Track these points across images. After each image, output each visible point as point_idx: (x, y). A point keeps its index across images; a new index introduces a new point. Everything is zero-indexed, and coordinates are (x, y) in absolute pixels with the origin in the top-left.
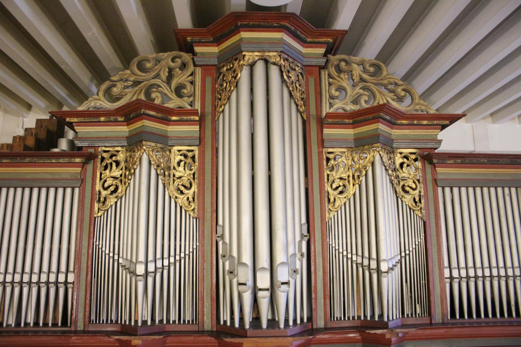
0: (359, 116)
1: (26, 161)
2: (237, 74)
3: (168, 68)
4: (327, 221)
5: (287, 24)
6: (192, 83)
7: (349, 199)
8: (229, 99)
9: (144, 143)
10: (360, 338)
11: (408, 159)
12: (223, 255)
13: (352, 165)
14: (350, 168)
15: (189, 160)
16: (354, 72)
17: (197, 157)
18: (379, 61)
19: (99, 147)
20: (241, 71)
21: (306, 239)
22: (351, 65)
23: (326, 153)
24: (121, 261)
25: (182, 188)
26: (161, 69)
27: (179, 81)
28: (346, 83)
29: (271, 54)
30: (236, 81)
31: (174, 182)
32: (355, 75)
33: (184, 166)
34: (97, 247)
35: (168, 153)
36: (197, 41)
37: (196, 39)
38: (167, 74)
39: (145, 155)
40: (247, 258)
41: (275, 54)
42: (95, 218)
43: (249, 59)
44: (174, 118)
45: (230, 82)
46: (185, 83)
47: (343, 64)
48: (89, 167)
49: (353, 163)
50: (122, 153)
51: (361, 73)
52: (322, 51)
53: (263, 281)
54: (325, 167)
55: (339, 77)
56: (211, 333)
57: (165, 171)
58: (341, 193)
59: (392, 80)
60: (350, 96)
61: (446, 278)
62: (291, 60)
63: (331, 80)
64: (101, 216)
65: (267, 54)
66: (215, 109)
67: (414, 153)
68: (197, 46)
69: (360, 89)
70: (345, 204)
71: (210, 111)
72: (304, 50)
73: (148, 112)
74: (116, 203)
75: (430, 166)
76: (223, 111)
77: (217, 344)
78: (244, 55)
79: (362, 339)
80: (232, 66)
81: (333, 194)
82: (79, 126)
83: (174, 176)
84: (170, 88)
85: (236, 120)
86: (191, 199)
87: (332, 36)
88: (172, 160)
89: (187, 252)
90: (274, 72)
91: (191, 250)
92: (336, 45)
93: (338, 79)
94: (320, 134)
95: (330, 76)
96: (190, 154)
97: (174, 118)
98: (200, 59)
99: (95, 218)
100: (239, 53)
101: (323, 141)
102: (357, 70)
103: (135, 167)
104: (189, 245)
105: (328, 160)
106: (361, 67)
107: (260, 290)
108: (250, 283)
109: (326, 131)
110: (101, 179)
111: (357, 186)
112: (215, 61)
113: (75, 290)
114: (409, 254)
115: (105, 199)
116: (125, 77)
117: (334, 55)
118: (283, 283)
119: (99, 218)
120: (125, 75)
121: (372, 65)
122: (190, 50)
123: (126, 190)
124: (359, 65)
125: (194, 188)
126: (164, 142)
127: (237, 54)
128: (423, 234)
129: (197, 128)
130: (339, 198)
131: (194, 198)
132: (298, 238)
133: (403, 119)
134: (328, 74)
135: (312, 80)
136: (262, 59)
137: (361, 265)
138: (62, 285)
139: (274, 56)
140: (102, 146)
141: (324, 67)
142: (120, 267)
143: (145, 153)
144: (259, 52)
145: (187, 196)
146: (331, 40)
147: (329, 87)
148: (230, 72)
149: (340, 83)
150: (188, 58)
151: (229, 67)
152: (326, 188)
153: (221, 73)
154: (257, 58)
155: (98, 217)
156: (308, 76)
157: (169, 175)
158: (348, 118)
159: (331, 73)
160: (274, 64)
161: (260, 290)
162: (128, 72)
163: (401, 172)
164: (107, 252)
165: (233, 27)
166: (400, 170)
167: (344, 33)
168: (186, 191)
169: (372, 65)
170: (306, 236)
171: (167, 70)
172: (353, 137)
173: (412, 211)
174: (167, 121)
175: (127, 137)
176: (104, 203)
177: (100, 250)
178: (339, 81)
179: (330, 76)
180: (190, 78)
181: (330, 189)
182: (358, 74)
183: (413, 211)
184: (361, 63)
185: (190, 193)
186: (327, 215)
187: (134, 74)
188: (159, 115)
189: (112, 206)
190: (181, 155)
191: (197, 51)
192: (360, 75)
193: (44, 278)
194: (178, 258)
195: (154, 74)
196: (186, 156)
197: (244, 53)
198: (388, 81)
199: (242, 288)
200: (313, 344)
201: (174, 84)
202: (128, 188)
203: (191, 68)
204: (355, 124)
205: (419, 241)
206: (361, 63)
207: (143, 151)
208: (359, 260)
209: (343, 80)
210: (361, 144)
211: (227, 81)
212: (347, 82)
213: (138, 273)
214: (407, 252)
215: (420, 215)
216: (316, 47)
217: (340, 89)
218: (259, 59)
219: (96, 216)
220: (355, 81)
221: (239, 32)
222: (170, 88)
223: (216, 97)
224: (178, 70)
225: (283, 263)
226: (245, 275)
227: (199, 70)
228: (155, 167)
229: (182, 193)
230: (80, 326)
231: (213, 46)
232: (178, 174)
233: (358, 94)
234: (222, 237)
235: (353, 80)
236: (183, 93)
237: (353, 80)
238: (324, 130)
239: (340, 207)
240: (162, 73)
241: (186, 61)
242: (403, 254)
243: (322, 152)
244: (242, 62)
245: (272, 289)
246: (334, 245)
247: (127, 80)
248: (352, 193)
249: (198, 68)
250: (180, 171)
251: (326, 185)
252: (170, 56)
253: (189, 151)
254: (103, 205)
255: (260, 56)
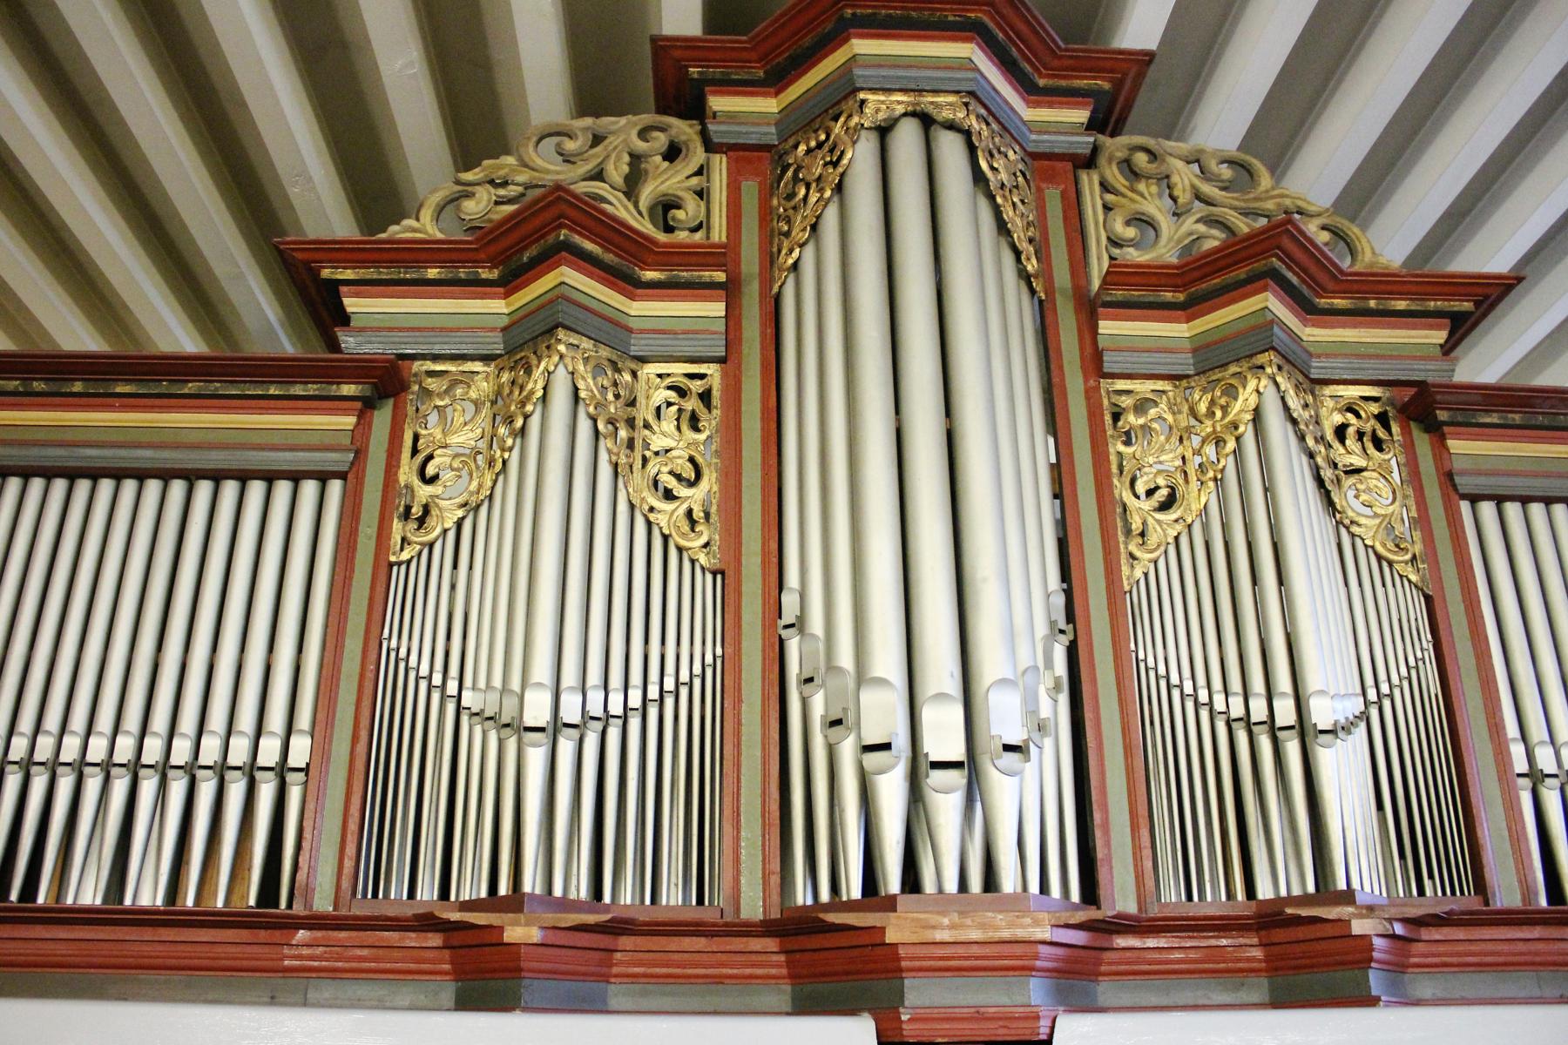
0: (1202, 278)
1: (186, 391)
2: (842, 153)
3: (631, 155)
4: (1127, 588)
5: (986, 20)
6: (700, 194)
7: (1189, 526)
8: (814, 227)
9: (561, 334)
10: (1257, 953)
11: (1358, 416)
12: (806, 675)
13: (1189, 429)
14: (1185, 436)
15: (691, 404)
16: (1175, 179)
17: (716, 393)
18: (1246, 153)
19: (413, 357)
20: (854, 143)
21: (1065, 640)
22: (1164, 161)
23: (1108, 392)
24: (468, 699)
25: (672, 483)
26: (608, 156)
27: (663, 188)
28: (1154, 206)
29: (940, 99)
30: (841, 170)
31: (644, 466)
32: (1180, 186)
33: (678, 420)
34: (393, 655)
35: (627, 377)
36: (718, 76)
37: (715, 72)
38: (626, 169)
39: (564, 369)
40: (887, 660)
41: (951, 99)
42: (391, 565)
43: (878, 111)
44: (650, 275)
45: (819, 180)
46: (680, 193)
47: (1141, 159)
48: (382, 418)
49: (1193, 422)
50: (486, 379)
51: (1197, 182)
52: (1081, 115)
53: (944, 740)
54: (1110, 432)
55: (1133, 190)
56: (767, 928)
57: (627, 419)
58: (1165, 506)
59: (1288, 202)
60: (1170, 240)
61: (1519, 775)
62: (995, 126)
63: (1109, 197)
64: (409, 562)
65: (930, 99)
66: (772, 263)
67: (1376, 399)
68: (715, 93)
69: (1198, 221)
70: (1177, 538)
71: (756, 269)
72: (1028, 113)
73: (577, 239)
74: (459, 525)
75: (1426, 436)
76: (795, 266)
77: (784, 971)
78: (863, 102)
79: (1267, 959)
80: (823, 137)
81: (1140, 508)
82: (357, 295)
83: (647, 446)
84: (636, 206)
85: (839, 278)
86: (698, 514)
87: (1112, 71)
88: (641, 400)
89: (684, 677)
90: (950, 148)
91: (697, 669)
92: (1122, 99)
93: (1130, 194)
94: (1088, 341)
95: (1105, 187)
96: (697, 386)
97: (650, 275)
98: (723, 128)
99: (391, 565)
100: (845, 98)
101: (1098, 356)
102: (1184, 177)
103: (529, 408)
104: (691, 651)
105: (1116, 417)
106: (1195, 167)
107: (937, 765)
108: (901, 742)
109: (1108, 327)
110: (415, 451)
111: (1211, 484)
112: (770, 134)
113: (312, 786)
114: (1391, 696)
115: (426, 510)
116: (502, 173)
117: (1112, 135)
118: (1008, 748)
119: (403, 568)
120: (500, 167)
121: (1231, 162)
122: (695, 110)
123: (495, 482)
124: (1188, 163)
125: (709, 483)
126: (621, 348)
127: (839, 102)
128: (1427, 636)
129: (718, 309)
130: (1158, 522)
131: (707, 516)
132: (1041, 629)
133: (1335, 293)
134: (1102, 184)
135: (1053, 196)
136: (914, 114)
137: (1242, 724)
138: (271, 775)
139: (950, 104)
140: (423, 357)
141: (1089, 161)
142: (465, 719)
143: (561, 367)
144: (904, 91)
145: (685, 506)
146: (1106, 86)
147: (1106, 215)
148: (820, 154)
149: (1137, 207)
150: (688, 130)
151: (813, 144)
152: (1116, 492)
153: (789, 165)
154: (900, 109)
155: (399, 564)
156: (1044, 186)
157: (631, 444)
158: (1176, 288)
159: (1110, 179)
160: (951, 126)
161: (937, 765)
162: (510, 160)
163: (1342, 450)
164: (424, 670)
165: (829, 26)
166: (1336, 444)
167: (1144, 59)
168: (681, 491)
169: (1231, 162)
170: (1062, 632)
171: (627, 158)
172: (1187, 345)
173: (1385, 564)
174: (630, 285)
175: (504, 329)
176: (421, 521)
177: (402, 665)
178: (1132, 200)
179: (1105, 187)
180: (695, 181)
181: (1127, 497)
182: (1187, 182)
183: (1390, 564)
184: (1195, 159)
185: (694, 497)
186: (1125, 570)
187: (526, 166)
188: (609, 258)
189: (445, 531)
190: (669, 388)
191: (715, 108)
192: (1193, 186)
193: (210, 751)
194: (653, 692)
195: (589, 166)
196: (682, 392)
197: (862, 95)
198: (1279, 205)
199: (872, 759)
200: (1327, 210)
201: (647, 194)
202: (501, 478)
203: (698, 156)
204: (1190, 308)
205: (1419, 655)
206: (1195, 159)
207: (556, 358)
208: (1237, 710)
209: (1142, 195)
210: (1215, 362)
211: (810, 178)
212: (1157, 202)
213: (529, 721)
214: (1385, 689)
215: (1413, 578)
216: (1061, 105)
217: (1141, 221)
218: (905, 114)
219: (393, 559)
220: (1180, 201)
221: (846, 40)
222: (636, 206)
223: (772, 231)
224: (658, 158)
225: (1003, 682)
226: (882, 714)
227: (720, 163)
228: (591, 409)
229: (669, 495)
230: (323, 903)
231: (765, 95)
232: (658, 443)
233: (1191, 234)
234: (799, 625)
235: (1174, 199)
236: (674, 219)
237: (1174, 199)
238: (1101, 323)
239: (1162, 549)
240: (610, 169)
241: (683, 138)
242: (1372, 695)
243: (1098, 388)
244: (855, 120)
245: (970, 765)
246: (1151, 663)
247: (505, 184)
248: (1196, 506)
249: (717, 157)
250: (665, 435)
251: (1116, 481)
252: (636, 124)
253: (692, 376)
254: (420, 528)
255: (908, 104)
